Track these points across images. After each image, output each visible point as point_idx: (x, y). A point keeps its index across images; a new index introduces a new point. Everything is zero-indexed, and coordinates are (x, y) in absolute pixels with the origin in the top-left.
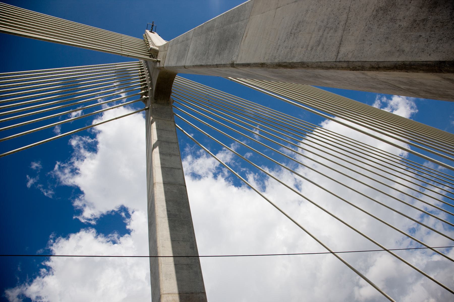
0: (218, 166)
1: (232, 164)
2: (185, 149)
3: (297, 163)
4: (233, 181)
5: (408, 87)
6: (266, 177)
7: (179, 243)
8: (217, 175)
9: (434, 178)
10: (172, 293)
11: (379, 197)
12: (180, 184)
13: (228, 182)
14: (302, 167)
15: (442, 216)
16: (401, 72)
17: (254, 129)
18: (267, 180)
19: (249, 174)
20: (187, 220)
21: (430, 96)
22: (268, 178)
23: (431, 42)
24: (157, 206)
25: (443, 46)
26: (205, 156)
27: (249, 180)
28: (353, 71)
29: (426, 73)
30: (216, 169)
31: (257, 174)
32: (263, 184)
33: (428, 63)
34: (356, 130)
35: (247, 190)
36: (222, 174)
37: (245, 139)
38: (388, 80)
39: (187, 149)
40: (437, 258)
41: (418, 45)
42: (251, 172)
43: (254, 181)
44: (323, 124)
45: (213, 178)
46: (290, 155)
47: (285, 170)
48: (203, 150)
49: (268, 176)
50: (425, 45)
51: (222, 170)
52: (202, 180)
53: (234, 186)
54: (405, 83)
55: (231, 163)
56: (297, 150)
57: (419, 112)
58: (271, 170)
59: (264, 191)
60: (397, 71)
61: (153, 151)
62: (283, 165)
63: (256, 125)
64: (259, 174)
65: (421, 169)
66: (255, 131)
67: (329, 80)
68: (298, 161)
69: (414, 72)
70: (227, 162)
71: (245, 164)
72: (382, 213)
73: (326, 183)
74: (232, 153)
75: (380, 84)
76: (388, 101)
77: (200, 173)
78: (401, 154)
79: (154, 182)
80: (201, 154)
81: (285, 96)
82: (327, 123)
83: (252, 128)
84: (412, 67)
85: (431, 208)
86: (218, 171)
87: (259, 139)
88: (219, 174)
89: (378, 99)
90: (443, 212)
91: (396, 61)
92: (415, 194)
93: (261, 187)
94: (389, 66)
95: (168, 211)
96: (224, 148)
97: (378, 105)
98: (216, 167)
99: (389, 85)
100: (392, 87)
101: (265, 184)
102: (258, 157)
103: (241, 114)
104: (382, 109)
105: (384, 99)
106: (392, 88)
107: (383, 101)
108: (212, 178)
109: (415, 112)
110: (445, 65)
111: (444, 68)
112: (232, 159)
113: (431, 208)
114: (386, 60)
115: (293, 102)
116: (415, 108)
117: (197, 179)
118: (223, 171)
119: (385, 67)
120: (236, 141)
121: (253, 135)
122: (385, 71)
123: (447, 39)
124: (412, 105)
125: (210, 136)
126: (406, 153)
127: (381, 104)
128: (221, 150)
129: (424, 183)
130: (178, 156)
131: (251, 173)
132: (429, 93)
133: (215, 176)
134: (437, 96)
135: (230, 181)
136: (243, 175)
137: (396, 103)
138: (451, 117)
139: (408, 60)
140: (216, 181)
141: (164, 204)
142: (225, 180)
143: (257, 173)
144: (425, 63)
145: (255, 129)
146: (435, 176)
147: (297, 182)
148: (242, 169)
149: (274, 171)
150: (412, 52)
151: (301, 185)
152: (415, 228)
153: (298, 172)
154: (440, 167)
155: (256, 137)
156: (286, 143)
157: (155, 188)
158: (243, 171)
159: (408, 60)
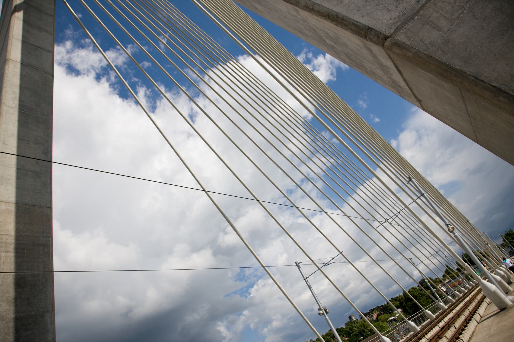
0: (104, 66)
1: (124, 69)
2: (65, 30)
3: (199, 91)
4: (119, 90)
5: (332, 44)
6: (159, 96)
7: (28, 144)
8: (101, 77)
9: (326, 148)
10: (7, 202)
11: (271, 152)
12: (45, 72)
13: (112, 89)
14: (203, 97)
15: (320, 184)
16: (331, 23)
17: (161, 36)
18: (160, 101)
19: (141, 87)
20: (46, 118)
22: (162, 98)
23: (369, 4)
24: (6, 91)
25: (377, 13)
26: (91, 48)
27: (139, 94)
28: (287, 2)
29: (353, 34)
30: (101, 70)
31: (150, 90)
32: (153, 104)
33: (358, 24)
34: (270, 74)
35: (134, 106)
36: (108, 77)
37: (147, 44)
38: (317, 27)
39: (69, 32)
40: (302, 220)
41: (357, 2)
42: (144, 85)
43: (144, 97)
44: (241, 59)
45: (95, 79)
46: (194, 81)
47: (184, 95)
48: (90, 40)
49: (162, 95)
50: (362, 4)
51: (108, 72)
52: (79, 78)
53: (118, 96)
54: (332, 38)
55: (122, 67)
56: (204, 77)
57: (336, 81)
58: (167, 90)
59: (153, 112)
60: (328, 21)
61: (14, 15)
62: (184, 88)
63: (166, 32)
64: (153, 91)
65: (318, 137)
66: (162, 39)
67: (260, 5)
68: (200, 88)
69: (343, 28)
70: (118, 65)
71: (139, 74)
72: (269, 168)
73: (224, 123)
74: (127, 55)
75: (308, 30)
77: (80, 67)
78: (305, 117)
79: (7, 58)
80: (86, 45)
81: (214, 14)
82: (245, 59)
83: (160, 34)
84: (343, 22)
85: (312, 175)
86: (104, 72)
87: (165, 50)
88: (103, 77)
89: (304, 53)
90: (322, 181)
91: (331, 10)
92: (304, 158)
93: (151, 106)
94: (323, 12)
95: (21, 100)
96: (118, 47)
97: (302, 59)
98: (102, 67)
99: (316, 35)
100: (318, 37)
101: (157, 105)
102: (157, 71)
103: (142, 4)
104: (304, 65)
105: (310, 55)
106: (318, 39)
107: (308, 56)
108: (94, 78)
109: (333, 80)
110: (371, 33)
111: (369, 35)
112: (125, 63)
113: (312, 175)
114: (322, 4)
115: (222, 24)
117: (74, 74)
118: (110, 74)
119: (319, 11)
120: (135, 43)
121: (159, 43)
122: (317, 16)
123: (383, 7)
124: (333, 72)
125: (102, 23)
126: (311, 116)
127: (306, 60)
128: (114, 48)
129: (316, 151)
130: (51, 34)
131: (143, 87)
132: (349, 58)
133: (98, 78)
134: (354, 64)
135: (115, 89)
136: (134, 86)
137: (319, 64)
138: (360, 96)
139: (342, 13)
140: (98, 83)
141: (17, 90)
142: (110, 85)
143: (151, 89)
144: (356, 23)
145: (162, 37)
146: (327, 146)
147: (192, 112)
148: (134, 78)
149: (171, 93)
150: (350, 6)
151: (196, 117)
152: (292, 190)
153: (197, 101)
154: (335, 140)
155: (162, 46)
156: (194, 65)
157: (7, 67)
158: (134, 81)
159: (342, 14)
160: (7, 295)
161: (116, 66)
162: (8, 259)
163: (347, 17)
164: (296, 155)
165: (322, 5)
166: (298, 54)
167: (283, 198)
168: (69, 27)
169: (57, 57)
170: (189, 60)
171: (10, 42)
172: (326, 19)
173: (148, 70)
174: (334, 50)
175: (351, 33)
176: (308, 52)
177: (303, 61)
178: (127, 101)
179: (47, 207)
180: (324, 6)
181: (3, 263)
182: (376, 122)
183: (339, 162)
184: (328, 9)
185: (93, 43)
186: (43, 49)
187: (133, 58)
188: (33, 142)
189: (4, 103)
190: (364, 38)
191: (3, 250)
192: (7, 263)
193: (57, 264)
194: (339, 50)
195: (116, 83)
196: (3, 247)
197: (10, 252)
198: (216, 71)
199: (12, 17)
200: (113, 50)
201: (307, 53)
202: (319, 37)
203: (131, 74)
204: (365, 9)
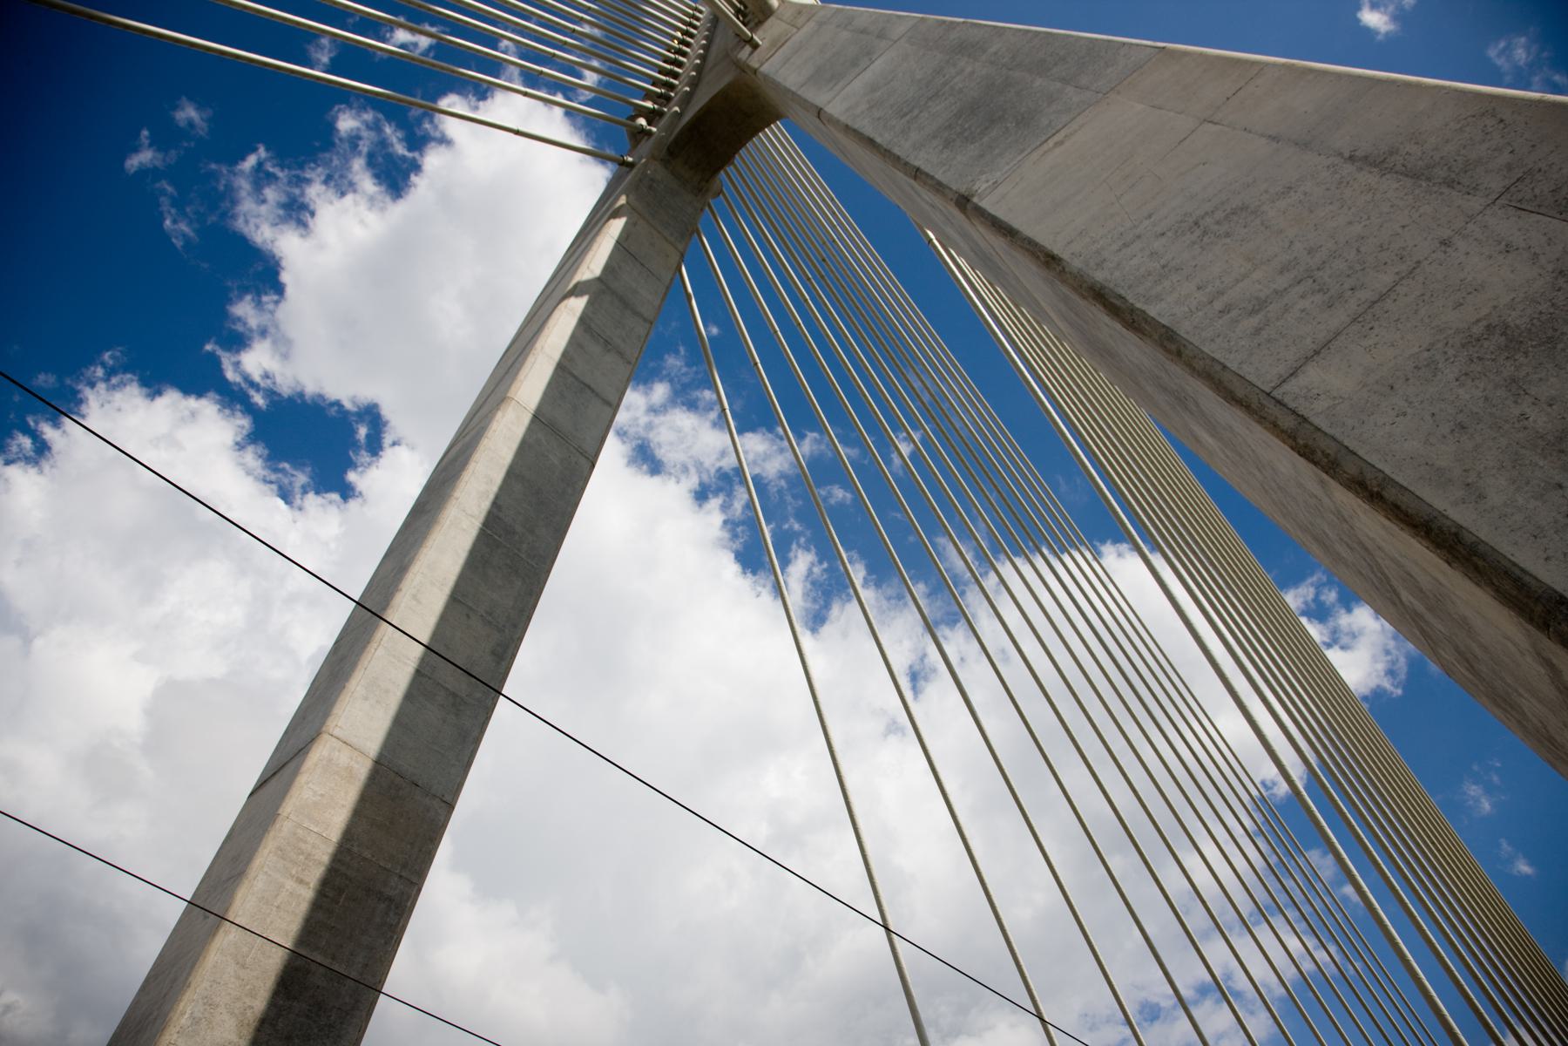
5: (1420, 608)
7: (468, 616)
8: (711, 496)
11: (1123, 862)
13: (726, 535)
16: (1431, 551)
18: (843, 605)
20: (535, 566)
21: (1462, 674)
22: (849, 600)
26: (713, 415)
28: (1301, 455)
29: (1500, 602)
30: (714, 476)
31: (825, 565)
33: (1527, 579)
35: (767, 597)
36: (727, 499)
39: (673, 362)
42: (812, 547)
44: (1110, 553)
48: (714, 397)
51: (731, 485)
52: (656, 480)
54: (1421, 590)
59: (814, 630)
60: (1424, 543)
61: (565, 302)
63: (916, 425)
64: (831, 570)
65: (1293, 862)
67: (1212, 436)
69: (1470, 578)
70: (764, 475)
71: (811, 515)
72: (1101, 910)
73: (1002, 724)
76: (1336, 609)
78: (1268, 783)
79: (509, 395)
84: (1475, 558)
85: (1242, 982)
86: (721, 484)
87: (901, 473)
89: (1312, 585)
91: (1440, 512)
92: (1226, 916)
94: (1410, 511)
95: (496, 504)
97: (1300, 600)
98: (720, 468)
99: (1369, 564)
100: (1376, 575)
104: (1304, 620)
105: (1331, 596)
106: (1375, 580)
107: (1323, 598)
108: (690, 491)
111: (1560, 624)
112: (782, 475)
113: (1242, 982)
114: (1412, 489)
116: (1398, 680)
117: (645, 467)
119: (1397, 507)
122: (1389, 519)
124: (1395, 668)
126: (1283, 788)
127: (1313, 606)
128: (771, 429)
130: (629, 363)
131: (808, 550)
132: (1467, 665)
133: (701, 495)
134: (1481, 687)
135: (735, 536)
136: (784, 544)
137: (1355, 628)
140: (697, 508)
141: (498, 477)
142: (725, 522)
144: (1518, 572)
148: (792, 520)
149: (880, 591)
150: (1506, 516)
151: (926, 679)
154: (1349, 890)
155: (897, 461)
157: (499, 414)
158: (791, 528)
159: (1476, 533)
160: (248, 1001)
161: (756, 479)
162: (294, 904)
163: (1491, 547)
164: (1203, 902)
165: (1410, 491)
166: (1291, 579)
167: (1123, 1024)
168: (677, 352)
169: (622, 417)
170: (958, 517)
171: (531, 359)
172: (1417, 535)
173: (838, 512)
174: (1422, 628)
175: (1495, 598)
176: (1324, 585)
177: (1303, 606)
178: (754, 578)
179: (444, 799)
180: (1417, 496)
181: (278, 907)
182: (1519, 872)
183: (1350, 972)
184: (1431, 506)
185: (720, 410)
186: (597, 395)
187: (809, 474)
188: (482, 616)
189: (457, 499)
190: (1538, 627)
191: (294, 872)
192: (288, 912)
193: (403, 973)
194: (1440, 631)
195: (743, 523)
196: (296, 863)
197: (308, 884)
198: (1026, 570)
199: (560, 306)
200: (767, 433)
201: (1321, 588)
202: (1379, 575)
203: (789, 508)
204: (1561, 538)
